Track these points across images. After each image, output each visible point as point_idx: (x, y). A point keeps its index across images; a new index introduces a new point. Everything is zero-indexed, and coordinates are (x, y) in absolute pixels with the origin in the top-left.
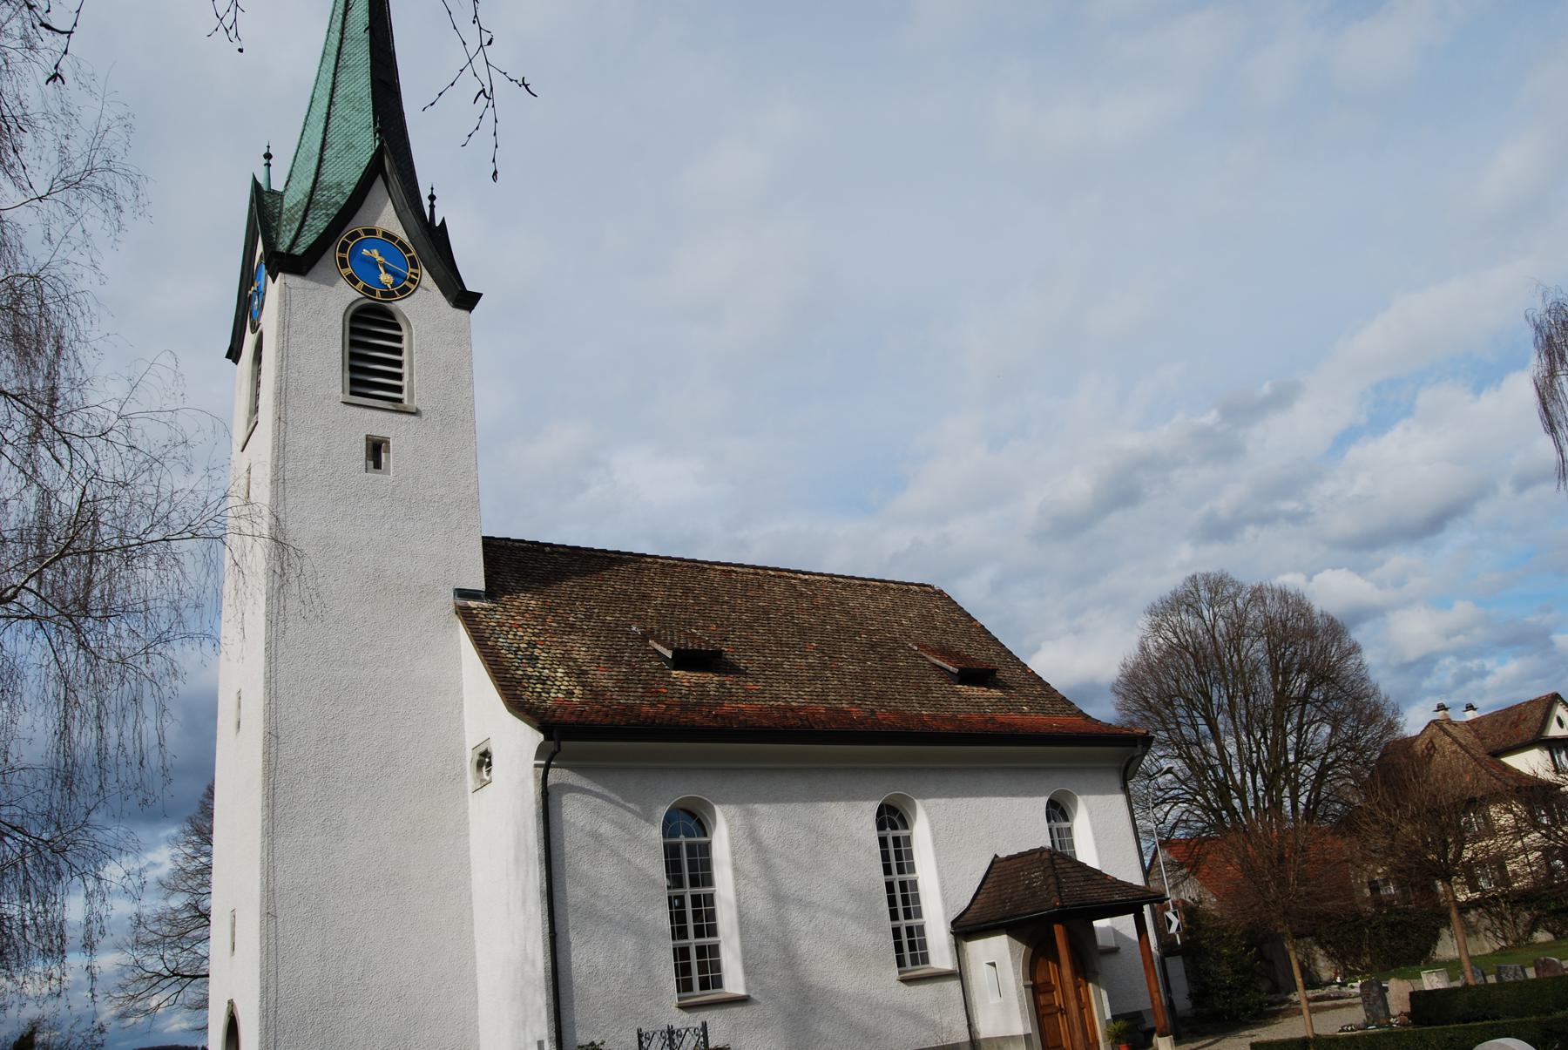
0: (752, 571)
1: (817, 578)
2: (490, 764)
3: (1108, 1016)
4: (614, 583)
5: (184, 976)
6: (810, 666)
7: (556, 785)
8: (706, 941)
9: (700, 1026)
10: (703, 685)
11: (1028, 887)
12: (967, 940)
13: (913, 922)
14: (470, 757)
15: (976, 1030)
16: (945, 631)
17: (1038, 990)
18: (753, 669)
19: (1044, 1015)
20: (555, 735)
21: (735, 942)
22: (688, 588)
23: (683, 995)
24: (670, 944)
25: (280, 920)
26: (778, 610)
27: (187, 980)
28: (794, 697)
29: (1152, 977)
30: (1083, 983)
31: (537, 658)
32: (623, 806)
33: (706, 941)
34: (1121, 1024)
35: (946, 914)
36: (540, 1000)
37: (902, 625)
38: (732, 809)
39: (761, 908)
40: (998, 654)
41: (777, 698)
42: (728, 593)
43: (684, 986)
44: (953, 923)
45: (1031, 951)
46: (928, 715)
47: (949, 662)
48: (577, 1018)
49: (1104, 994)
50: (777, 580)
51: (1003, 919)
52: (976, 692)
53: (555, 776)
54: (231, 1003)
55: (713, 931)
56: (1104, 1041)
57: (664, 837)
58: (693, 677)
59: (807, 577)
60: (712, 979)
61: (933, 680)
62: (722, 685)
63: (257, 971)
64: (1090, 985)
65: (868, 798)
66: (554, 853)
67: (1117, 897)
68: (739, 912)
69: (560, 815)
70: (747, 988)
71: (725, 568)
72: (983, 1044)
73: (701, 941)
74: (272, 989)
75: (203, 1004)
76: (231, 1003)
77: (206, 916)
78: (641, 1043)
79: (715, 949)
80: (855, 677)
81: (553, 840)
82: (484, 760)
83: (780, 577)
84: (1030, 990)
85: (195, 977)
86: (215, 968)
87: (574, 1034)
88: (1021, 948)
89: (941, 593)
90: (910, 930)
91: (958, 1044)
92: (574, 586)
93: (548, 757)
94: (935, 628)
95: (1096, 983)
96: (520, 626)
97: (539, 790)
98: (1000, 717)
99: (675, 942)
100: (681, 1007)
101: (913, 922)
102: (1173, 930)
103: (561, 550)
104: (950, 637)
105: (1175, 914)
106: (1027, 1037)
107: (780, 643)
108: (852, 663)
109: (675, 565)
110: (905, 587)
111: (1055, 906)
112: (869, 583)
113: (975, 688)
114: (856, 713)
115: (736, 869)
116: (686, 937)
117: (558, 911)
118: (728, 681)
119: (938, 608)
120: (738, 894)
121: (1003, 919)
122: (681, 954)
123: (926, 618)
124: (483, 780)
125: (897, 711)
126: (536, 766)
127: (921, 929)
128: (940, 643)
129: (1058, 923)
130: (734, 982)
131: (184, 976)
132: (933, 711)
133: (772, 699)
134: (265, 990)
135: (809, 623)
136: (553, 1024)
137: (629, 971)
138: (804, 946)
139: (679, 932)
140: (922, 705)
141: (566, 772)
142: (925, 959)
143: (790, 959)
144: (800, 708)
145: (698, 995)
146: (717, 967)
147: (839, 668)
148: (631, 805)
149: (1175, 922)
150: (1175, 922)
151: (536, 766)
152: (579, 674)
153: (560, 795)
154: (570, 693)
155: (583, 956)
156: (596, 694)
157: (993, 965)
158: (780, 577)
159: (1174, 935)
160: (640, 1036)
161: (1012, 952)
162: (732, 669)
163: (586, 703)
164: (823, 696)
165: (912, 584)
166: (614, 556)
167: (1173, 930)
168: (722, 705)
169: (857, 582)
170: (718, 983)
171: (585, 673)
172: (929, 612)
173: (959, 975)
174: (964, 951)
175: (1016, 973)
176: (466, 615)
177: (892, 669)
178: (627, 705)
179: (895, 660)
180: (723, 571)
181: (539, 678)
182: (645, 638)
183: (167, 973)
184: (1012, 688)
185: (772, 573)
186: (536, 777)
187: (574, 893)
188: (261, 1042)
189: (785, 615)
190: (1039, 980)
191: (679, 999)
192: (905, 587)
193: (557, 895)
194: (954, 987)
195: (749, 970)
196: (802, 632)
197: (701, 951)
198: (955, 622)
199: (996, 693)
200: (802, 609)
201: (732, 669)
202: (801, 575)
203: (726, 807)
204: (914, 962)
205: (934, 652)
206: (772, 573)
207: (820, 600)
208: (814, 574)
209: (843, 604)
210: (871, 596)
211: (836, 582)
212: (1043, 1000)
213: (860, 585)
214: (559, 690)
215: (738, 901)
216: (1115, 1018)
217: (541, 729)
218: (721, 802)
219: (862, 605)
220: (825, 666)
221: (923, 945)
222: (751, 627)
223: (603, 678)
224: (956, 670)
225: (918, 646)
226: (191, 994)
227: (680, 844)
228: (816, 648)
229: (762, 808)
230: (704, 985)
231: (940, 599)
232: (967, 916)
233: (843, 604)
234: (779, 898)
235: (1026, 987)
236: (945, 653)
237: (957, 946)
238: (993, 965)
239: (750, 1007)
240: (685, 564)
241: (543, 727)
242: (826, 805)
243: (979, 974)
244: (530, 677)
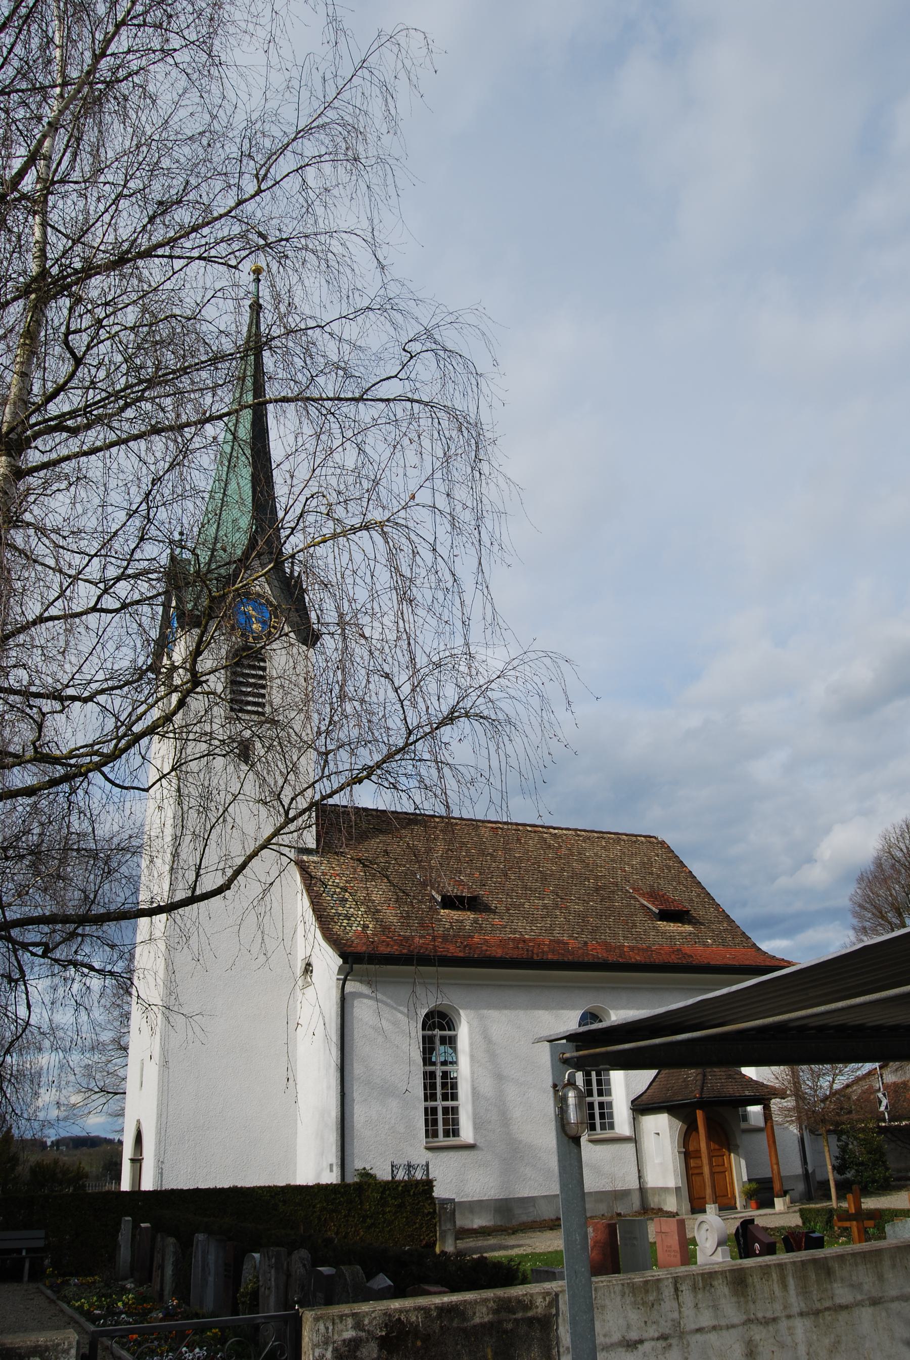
0: (514, 827)
1: (564, 832)
2: (312, 972)
3: (745, 1178)
4: (411, 837)
5: (109, 1093)
6: (545, 906)
7: (351, 993)
8: (449, 1103)
9: (424, 1163)
10: (462, 921)
11: (685, 1080)
12: (642, 1115)
13: (604, 1099)
14: (299, 967)
15: (644, 1181)
16: (658, 876)
17: (688, 1154)
18: (501, 908)
19: (692, 1174)
20: (350, 961)
21: (469, 1107)
22: (463, 843)
23: (430, 1140)
24: (422, 1105)
25: (171, 1071)
26: (528, 860)
27: (111, 1095)
28: (525, 930)
29: (773, 1153)
30: (727, 1153)
31: (347, 900)
32: (396, 1009)
33: (449, 1103)
34: (754, 1185)
35: (628, 1095)
36: (332, 1138)
37: (625, 871)
38: (471, 1013)
39: (487, 1086)
40: (699, 895)
41: (514, 932)
42: (493, 846)
43: (431, 1133)
44: (632, 1102)
45: (686, 1127)
46: (629, 947)
47: (653, 904)
48: (356, 1151)
49: (743, 1162)
50: (533, 835)
51: (664, 1102)
52: (672, 927)
53: (350, 987)
54: (139, 1122)
55: (454, 1097)
56: (740, 1197)
57: (424, 1029)
58: (455, 915)
59: (556, 831)
60: (453, 1130)
61: (639, 917)
62: (475, 921)
63: (155, 1103)
64: (732, 1155)
65: (573, 1008)
66: (346, 1039)
67: (747, 1093)
68: (473, 1085)
69: (352, 1013)
70: (475, 1139)
71: (494, 825)
72: (649, 1191)
73: (446, 1103)
74: (164, 1116)
75: (121, 1114)
76: (139, 1122)
77: (125, 1049)
78: (393, 1171)
79: (455, 1110)
80: (578, 914)
81: (346, 1030)
82: (308, 968)
83: (535, 832)
84: (683, 1155)
85: (116, 1094)
86: (131, 1086)
87: (353, 1161)
88: (678, 1124)
89: (663, 843)
90: (601, 1105)
91: (630, 1190)
92: (379, 843)
93: (346, 973)
94: (652, 874)
95: (737, 1154)
96: (338, 875)
97: (339, 996)
98: (687, 949)
99: (427, 1103)
100: (428, 1148)
101: (604, 1099)
102: (882, 1108)
103: (374, 813)
104: (662, 882)
105: (884, 1094)
106: (678, 1189)
107: (525, 888)
108: (578, 904)
109: (456, 824)
110: (634, 839)
111: (695, 1097)
112: (605, 835)
113: (672, 924)
114: (573, 944)
115: (472, 1057)
116: (436, 1100)
117: (346, 1078)
118: (480, 917)
119: (658, 856)
120: (473, 1073)
121: (664, 1102)
122: (430, 1113)
123: (646, 865)
124: (308, 982)
125: (605, 944)
126: (338, 979)
127: (610, 1104)
128: (652, 887)
129: (700, 1109)
130: (467, 1134)
131: (109, 1093)
132: (633, 943)
133: (511, 932)
134: (160, 1116)
135: (551, 870)
136: (339, 1153)
137: (393, 1121)
138: (517, 1113)
139: (430, 1096)
140: (625, 938)
141: (358, 984)
142: (612, 1127)
143: (505, 1119)
144: (530, 940)
145: (441, 1140)
146: (456, 1122)
147: (566, 908)
148: (401, 1008)
149: (885, 1102)
150: (885, 1102)
151: (338, 979)
152: (374, 912)
153: (353, 1000)
154: (365, 927)
155: (360, 1114)
156: (385, 928)
157: (658, 1134)
158: (535, 832)
159: (883, 1113)
160: (392, 1166)
161: (671, 1127)
162: (487, 909)
163: (376, 935)
164: (550, 930)
165: (640, 836)
166: (412, 817)
167: (882, 1108)
168: (473, 937)
169: (596, 835)
170: (456, 1133)
171: (378, 911)
172: (649, 860)
173: (634, 1140)
174: (639, 1123)
175: (672, 1142)
176: (303, 867)
177: (608, 908)
178: (404, 937)
179: (612, 901)
180: (492, 828)
181: (346, 916)
182: (424, 884)
183: (97, 1090)
184: (702, 924)
185: (529, 829)
186: (337, 987)
187: (357, 1069)
188: (155, 1150)
189: (533, 864)
190: (691, 1148)
191: (427, 1143)
192: (634, 839)
193: (347, 1067)
194: (631, 1147)
195: (477, 1126)
196: (544, 878)
197: (446, 1110)
198: (669, 868)
199: (688, 928)
200: (548, 860)
201: (487, 909)
202: (551, 830)
203: (468, 1011)
204: (603, 1128)
205: (643, 895)
206: (529, 829)
207: (564, 851)
208: (562, 829)
209: (581, 854)
210: (604, 847)
211: (579, 836)
212: (693, 1163)
213: (598, 838)
214: (359, 925)
215: (472, 1077)
216: (750, 1180)
217: (341, 956)
218: (465, 1008)
219: (596, 855)
220: (556, 906)
221: (611, 1116)
222: (506, 875)
223: (391, 915)
224: (657, 911)
225: (634, 889)
226: (113, 1106)
227: (435, 1036)
228: (552, 892)
229: (493, 1014)
230: (447, 1134)
231: (662, 848)
232: (644, 1097)
233: (581, 854)
234: (499, 1077)
235: (679, 1152)
236: (653, 895)
237: (634, 1119)
238: (658, 1134)
239: (476, 1152)
240: (464, 822)
241: (342, 955)
242: (541, 1012)
243: (649, 1143)
244: (340, 915)
